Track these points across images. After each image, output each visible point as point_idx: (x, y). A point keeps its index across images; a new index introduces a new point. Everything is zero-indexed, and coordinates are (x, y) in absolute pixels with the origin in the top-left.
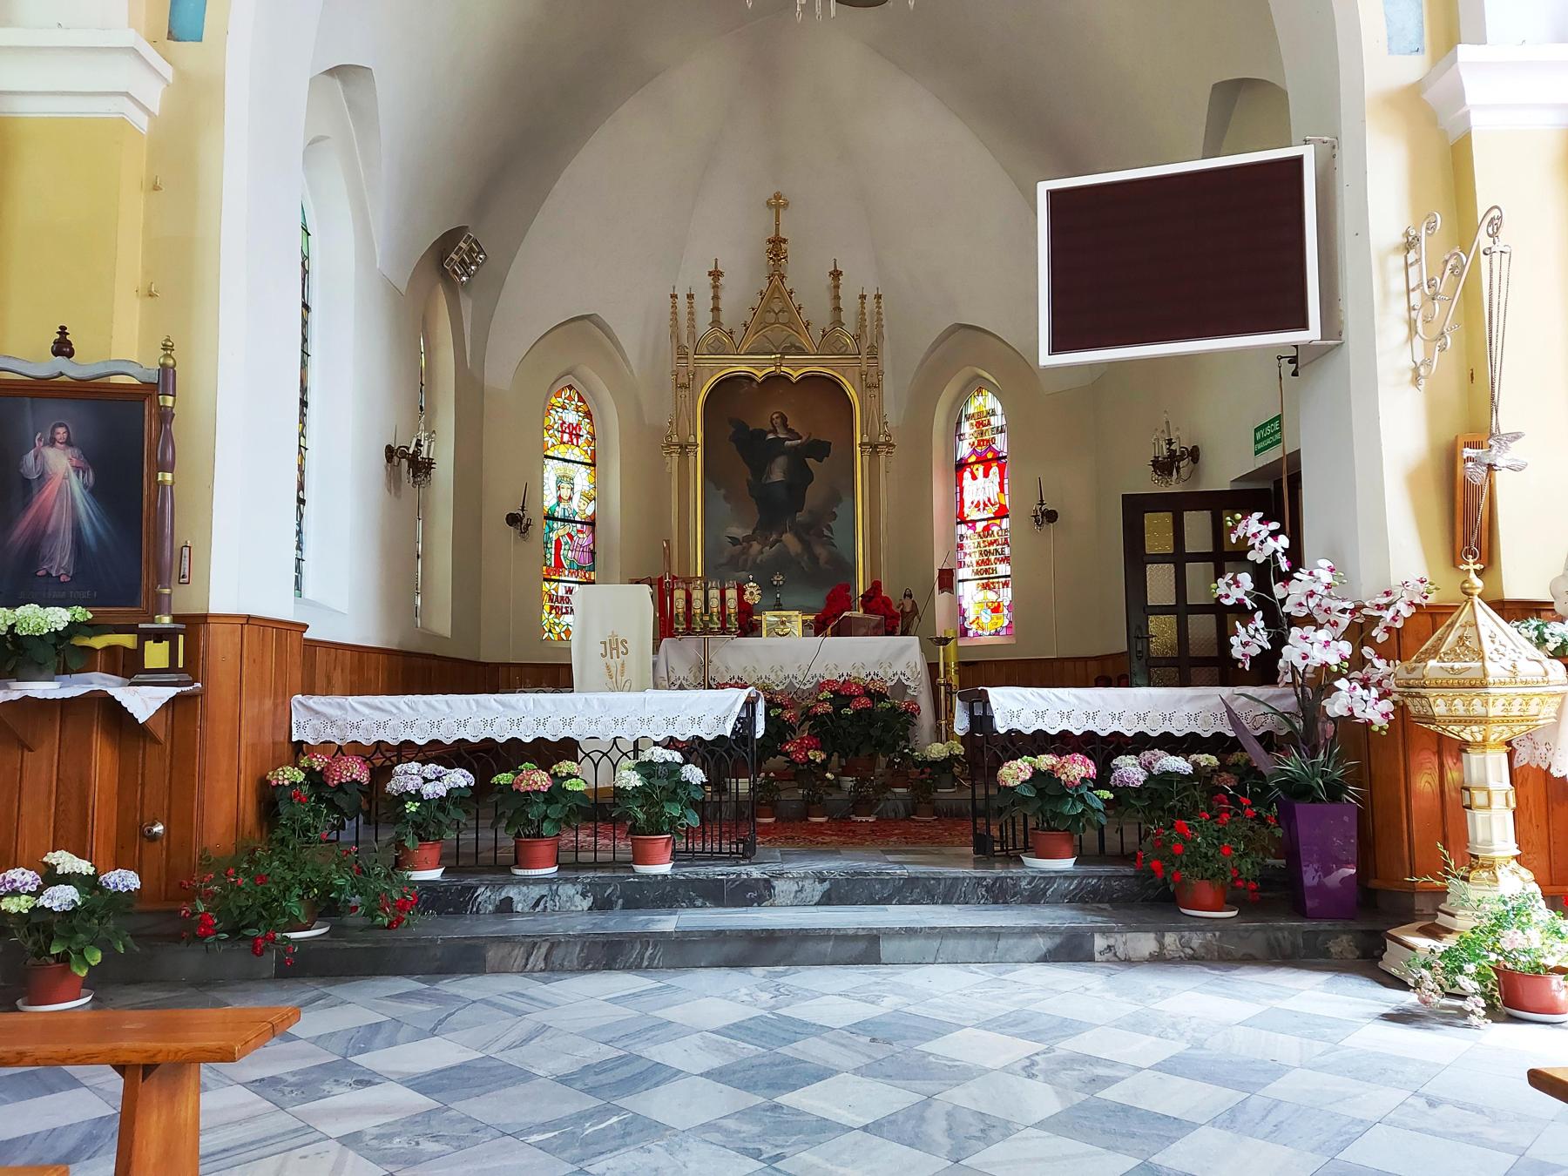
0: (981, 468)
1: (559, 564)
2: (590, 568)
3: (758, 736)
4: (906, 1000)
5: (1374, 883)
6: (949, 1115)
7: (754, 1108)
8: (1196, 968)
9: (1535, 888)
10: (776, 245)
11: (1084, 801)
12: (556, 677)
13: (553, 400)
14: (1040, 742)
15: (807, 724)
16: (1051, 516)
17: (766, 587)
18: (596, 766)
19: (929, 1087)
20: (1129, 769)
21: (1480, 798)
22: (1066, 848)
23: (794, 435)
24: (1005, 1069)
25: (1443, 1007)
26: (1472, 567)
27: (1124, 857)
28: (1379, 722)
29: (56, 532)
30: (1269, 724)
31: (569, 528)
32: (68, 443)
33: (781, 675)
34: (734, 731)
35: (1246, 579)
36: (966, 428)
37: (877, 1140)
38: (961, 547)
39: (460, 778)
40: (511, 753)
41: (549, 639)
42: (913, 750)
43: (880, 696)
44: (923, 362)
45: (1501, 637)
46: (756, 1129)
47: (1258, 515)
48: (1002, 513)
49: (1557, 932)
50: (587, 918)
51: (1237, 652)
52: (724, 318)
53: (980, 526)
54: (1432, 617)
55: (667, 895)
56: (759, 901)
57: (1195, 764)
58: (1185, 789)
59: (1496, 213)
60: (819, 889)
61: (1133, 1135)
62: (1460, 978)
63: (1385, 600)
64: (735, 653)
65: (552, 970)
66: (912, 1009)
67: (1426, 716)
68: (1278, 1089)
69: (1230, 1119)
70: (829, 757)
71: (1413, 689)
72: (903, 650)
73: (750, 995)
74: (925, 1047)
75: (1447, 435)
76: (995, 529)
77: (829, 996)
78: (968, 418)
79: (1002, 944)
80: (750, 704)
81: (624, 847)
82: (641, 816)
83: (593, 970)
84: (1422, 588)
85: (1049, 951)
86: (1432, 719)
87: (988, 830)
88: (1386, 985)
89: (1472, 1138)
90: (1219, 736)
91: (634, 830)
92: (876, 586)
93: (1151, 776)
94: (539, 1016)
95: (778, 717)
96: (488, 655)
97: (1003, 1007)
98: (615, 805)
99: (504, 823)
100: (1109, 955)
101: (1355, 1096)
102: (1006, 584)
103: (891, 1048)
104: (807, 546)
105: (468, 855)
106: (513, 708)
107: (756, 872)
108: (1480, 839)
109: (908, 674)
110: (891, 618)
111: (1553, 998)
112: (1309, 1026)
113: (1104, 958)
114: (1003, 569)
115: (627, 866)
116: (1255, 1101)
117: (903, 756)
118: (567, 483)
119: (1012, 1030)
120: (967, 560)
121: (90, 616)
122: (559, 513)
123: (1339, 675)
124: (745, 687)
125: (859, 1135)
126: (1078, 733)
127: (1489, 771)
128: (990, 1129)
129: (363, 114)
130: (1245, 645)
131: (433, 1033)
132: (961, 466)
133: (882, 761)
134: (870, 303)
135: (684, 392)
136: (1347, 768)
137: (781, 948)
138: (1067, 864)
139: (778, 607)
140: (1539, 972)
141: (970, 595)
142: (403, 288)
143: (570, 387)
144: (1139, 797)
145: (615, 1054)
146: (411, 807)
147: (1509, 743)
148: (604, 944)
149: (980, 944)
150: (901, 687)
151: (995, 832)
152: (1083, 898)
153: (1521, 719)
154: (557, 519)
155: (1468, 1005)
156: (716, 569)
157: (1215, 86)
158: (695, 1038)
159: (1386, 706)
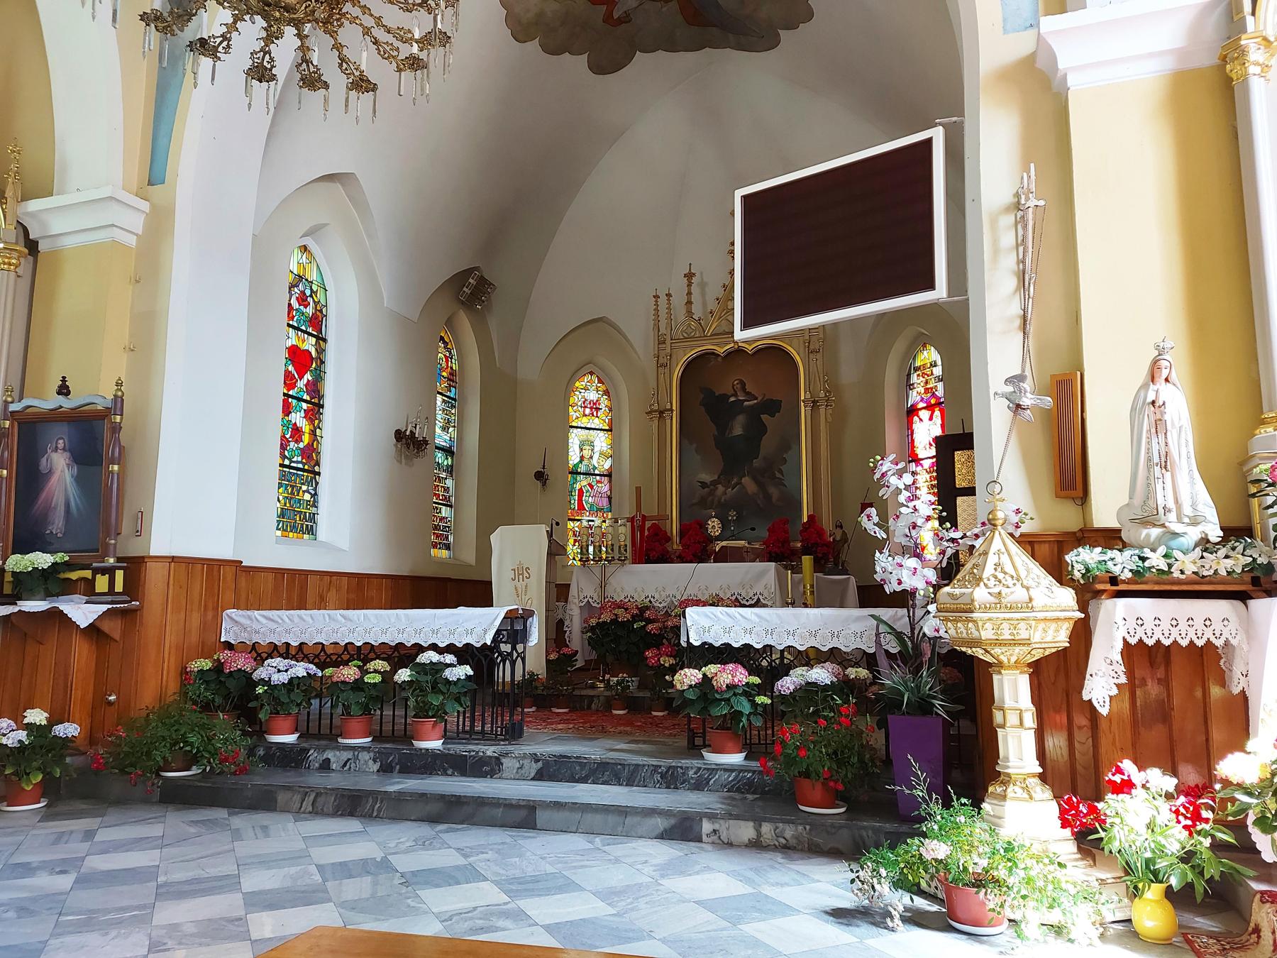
1: (581, 507)
14: (724, 654)
20: (787, 684)
23: (751, 396)
29: (56, 505)
31: (591, 479)
32: (64, 449)
33: (664, 594)
60: (536, 767)
65: (317, 813)
72: (762, 574)
78: (916, 369)
79: (629, 820)
83: (342, 815)
85: (665, 830)
100: (715, 838)
105: (1056, 727)
109: (766, 594)
113: (710, 840)
121: (67, 558)
122: (582, 468)
129: (359, 202)
138: (736, 759)
142: (415, 316)
143: (591, 373)
149: (612, 819)
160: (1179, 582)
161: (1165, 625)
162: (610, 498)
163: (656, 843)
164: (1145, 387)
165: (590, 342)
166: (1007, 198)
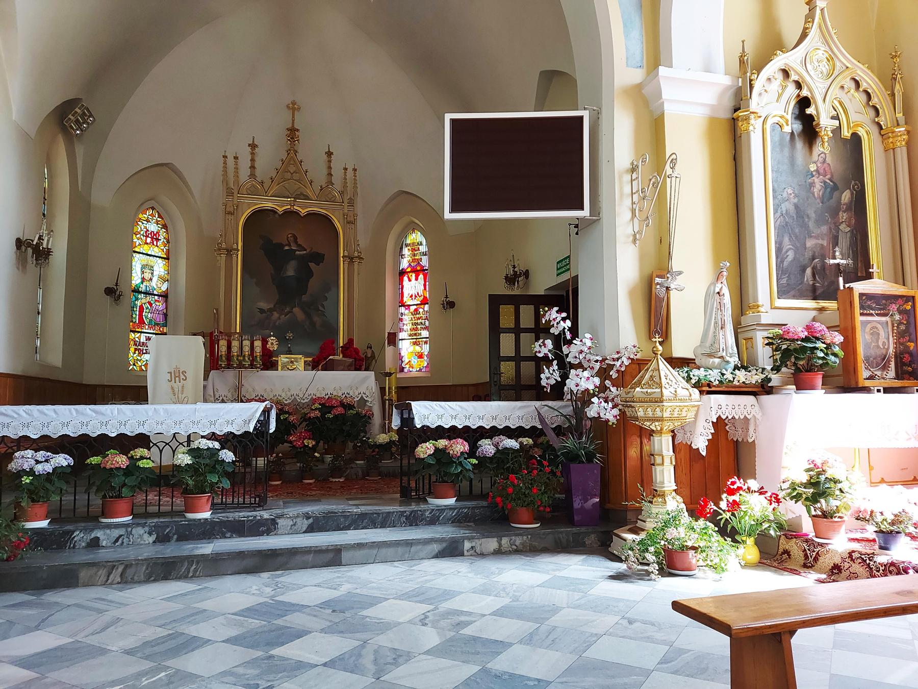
0: (414, 275)
1: (141, 321)
2: (164, 324)
3: (271, 431)
4: (355, 586)
5: (608, 506)
6: (376, 652)
7: (256, 659)
8: (517, 557)
9: (683, 506)
10: (292, 133)
11: (462, 466)
12: (135, 393)
13: (141, 216)
14: (439, 432)
15: (304, 424)
16: (451, 305)
17: (282, 340)
18: (161, 451)
19: (364, 636)
20: (487, 447)
21: (658, 460)
22: (452, 492)
24: (410, 622)
25: (639, 570)
26: (657, 340)
27: (483, 496)
28: (612, 420)
30: (559, 421)
31: (149, 298)
33: (289, 394)
34: (255, 428)
35: (549, 343)
36: (406, 251)
37: (331, 671)
38: (401, 320)
39: (63, 460)
40: (102, 443)
41: (133, 370)
42: (369, 438)
43: (350, 407)
44: (382, 210)
45: (670, 376)
46: (256, 672)
47: (556, 309)
48: (424, 302)
49: (693, 528)
50: (152, 548)
51: (543, 383)
52: (258, 172)
53: (412, 308)
54: (639, 364)
55: (207, 531)
56: (268, 532)
57: (521, 443)
58: (515, 457)
59: (674, 156)
60: (306, 523)
61: (478, 653)
62: (647, 555)
63: (617, 356)
64: (259, 380)
65: (126, 582)
66: (358, 591)
67: (634, 417)
68: (556, 620)
69: (529, 640)
70: (317, 443)
71: (628, 403)
72: (365, 379)
73: (259, 590)
74: (365, 613)
75: (648, 271)
76: (421, 310)
77: (309, 587)
78: (407, 245)
79: (413, 549)
80: (266, 412)
81: (179, 501)
82: (190, 482)
83: (155, 581)
84: (634, 350)
85: (439, 552)
86: (637, 419)
87: (409, 484)
88: (612, 560)
89: (650, 639)
90: (534, 428)
91: (186, 492)
92: (351, 341)
93: (498, 451)
94: (114, 613)
95: (286, 419)
96: (90, 378)
97: (412, 586)
98: (173, 476)
99: (95, 488)
100: (472, 552)
101: (593, 621)
102: (426, 343)
103: (343, 615)
104: (308, 316)
106: (103, 414)
107: (266, 515)
108: (658, 481)
109: (367, 394)
110: (358, 360)
111: (690, 562)
112: (573, 584)
113: (469, 554)
114: (425, 334)
115: (181, 514)
116: (544, 628)
117: (363, 442)
118: (149, 268)
119: (415, 599)
120: (405, 327)
122: (143, 288)
123: (594, 395)
124: (264, 401)
125: (320, 669)
126: (460, 427)
127: (664, 445)
128: (399, 657)
130: (548, 378)
131: (37, 628)
132: (402, 273)
133: (351, 445)
134: (350, 173)
135: (230, 217)
136: (596, 445)
137: (280, 560)
138: (451, 501)
139: (289, 352)
140: (684, 548)
141: (406, 348)
142: (33, 132)
143: (153, 208)
144: (491, 463)
145: (166, 633)
146: (26, 480)
147: (673, 431)
148: (163, 564)
149: (400, 550)
150: (363, 402)
151: (413, 484)
152: (459, 520)
153: (678, 419)
154: (141, 292)
155: (650, 568)
156: (248, 328)
157: (542, 73)
158: (221, 619)
159: (616, 412)
160: (736, 387)
161: (730, 408)
162: (165, 315)
163: (434, 561)
164: (713, 284)
165: (158, 182)
166: (628, 165)
